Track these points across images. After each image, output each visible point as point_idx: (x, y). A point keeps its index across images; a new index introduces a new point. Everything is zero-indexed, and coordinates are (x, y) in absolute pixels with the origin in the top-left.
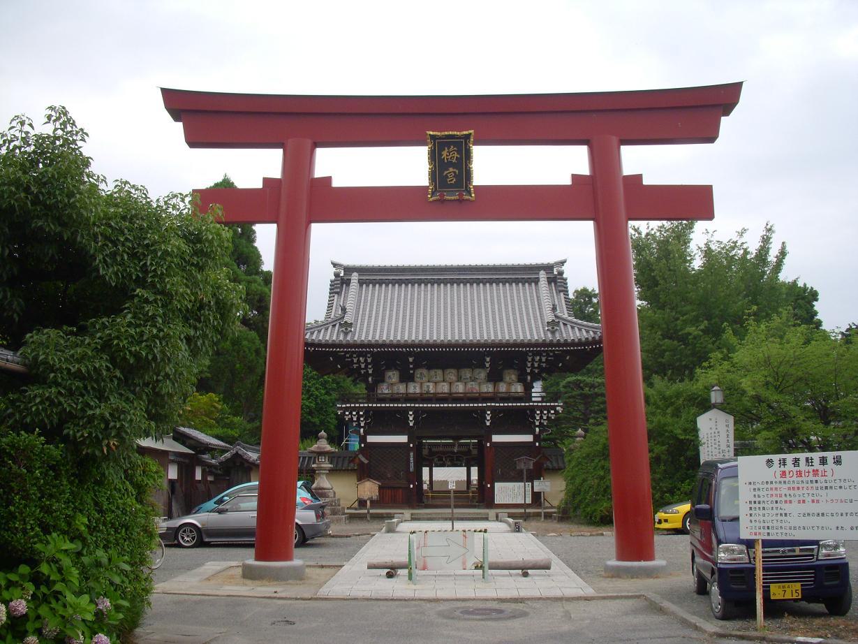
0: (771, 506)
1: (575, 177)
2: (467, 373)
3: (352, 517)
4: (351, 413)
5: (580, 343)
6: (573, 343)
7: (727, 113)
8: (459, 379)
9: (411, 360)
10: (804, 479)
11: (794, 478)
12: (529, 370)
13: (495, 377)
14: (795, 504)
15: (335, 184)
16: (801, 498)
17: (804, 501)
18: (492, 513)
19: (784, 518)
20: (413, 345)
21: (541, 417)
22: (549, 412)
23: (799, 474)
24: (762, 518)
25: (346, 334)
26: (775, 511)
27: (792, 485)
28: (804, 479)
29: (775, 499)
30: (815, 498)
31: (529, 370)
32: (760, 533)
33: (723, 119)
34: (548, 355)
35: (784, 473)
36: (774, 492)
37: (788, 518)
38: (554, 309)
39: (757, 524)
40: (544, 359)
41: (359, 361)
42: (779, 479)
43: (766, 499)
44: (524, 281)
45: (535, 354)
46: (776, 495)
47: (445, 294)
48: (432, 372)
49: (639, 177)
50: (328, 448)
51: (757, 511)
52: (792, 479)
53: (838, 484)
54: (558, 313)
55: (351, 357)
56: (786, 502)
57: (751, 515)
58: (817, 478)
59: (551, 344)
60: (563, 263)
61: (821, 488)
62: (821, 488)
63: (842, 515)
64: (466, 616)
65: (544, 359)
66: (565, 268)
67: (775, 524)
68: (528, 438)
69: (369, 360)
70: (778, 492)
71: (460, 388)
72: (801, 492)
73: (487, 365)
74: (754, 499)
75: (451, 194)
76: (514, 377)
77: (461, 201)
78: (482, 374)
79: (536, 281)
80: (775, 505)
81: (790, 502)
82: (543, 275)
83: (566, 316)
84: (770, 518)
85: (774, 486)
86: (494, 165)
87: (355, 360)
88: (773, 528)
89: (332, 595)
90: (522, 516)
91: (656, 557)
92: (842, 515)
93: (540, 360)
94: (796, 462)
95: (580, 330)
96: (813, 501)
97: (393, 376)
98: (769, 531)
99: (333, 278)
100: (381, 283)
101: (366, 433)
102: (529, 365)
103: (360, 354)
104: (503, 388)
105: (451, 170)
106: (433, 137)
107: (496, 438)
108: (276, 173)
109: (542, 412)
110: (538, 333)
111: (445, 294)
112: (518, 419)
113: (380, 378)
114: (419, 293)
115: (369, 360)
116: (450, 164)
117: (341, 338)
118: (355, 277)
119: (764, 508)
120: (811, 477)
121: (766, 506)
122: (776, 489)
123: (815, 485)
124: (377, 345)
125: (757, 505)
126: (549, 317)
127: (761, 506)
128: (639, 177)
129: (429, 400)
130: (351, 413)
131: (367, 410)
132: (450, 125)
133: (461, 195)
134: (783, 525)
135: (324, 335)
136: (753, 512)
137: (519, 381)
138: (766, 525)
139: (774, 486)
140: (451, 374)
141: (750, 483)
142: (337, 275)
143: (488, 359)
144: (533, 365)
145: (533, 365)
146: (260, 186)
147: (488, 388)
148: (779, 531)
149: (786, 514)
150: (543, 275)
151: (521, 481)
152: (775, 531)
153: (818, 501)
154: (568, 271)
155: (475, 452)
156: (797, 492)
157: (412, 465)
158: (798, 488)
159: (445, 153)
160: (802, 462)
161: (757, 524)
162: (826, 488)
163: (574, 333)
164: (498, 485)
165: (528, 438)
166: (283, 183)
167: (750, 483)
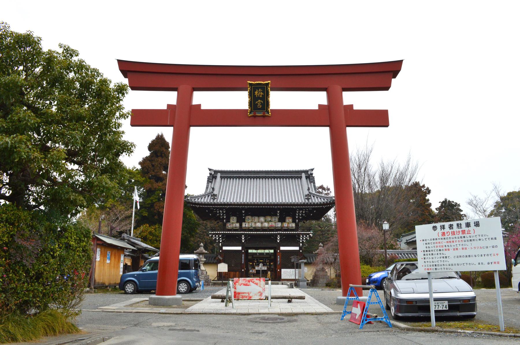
0: (436, 252)
1: (320, 106)
2: (269, 218)
3: (214, 284)
4: (215, 236)
5: (320, 204)
6: (317, 204)
7: (395, 76)
8: (266, 221)
9: (243, 212)
10: (457, 236)
11: (450, 236)
12: (297, 217)
13: (282, 220)
14: (451, 251)
15: (203, 108)
16: (455, 247)
17: (457, 249)
18: (280, 282)
19: (445, 259)
20: (244, 205)
21: (303, 239)
22: (306, 236)
23: (453, 233)
24: (431, 260)
25: (214, 199)
26: (439, 256)
27: (449, 240)
28: (457, 236)
29: (439, 248)
30: (464, 247)
31: (297, 217)
32: (431, 269)
33: (393, 79)
34: (306, 210)
35: (444, 234)
36: (438, 245)
37: (447, 259)
38: (309, 189)
39: (429, 264)
40: (304, 212)
41: (220, 212)
42: (441, 237)
43: (433, 249)
44: (295, 178)
45: (300, 209)
46: (440, 246)
47: (260, 183)
48: (253, 218)
49: (352, 106)
50: (204, 251)
51: (429, 256)
52: (449, 237)
53: (478, 238)
54: (311, 191)
55: (216, 210)
56: (446, 250)
57: (425, 258)
58: (464, 235)
59: (307, 205)
60: (312, 170)
61: (468, 241)
62: (468, 241)
63: (481, 255)
64: (264, 321)
65: (304, 212)
66: (313, 172)
67: (440, 263)
68: (297, 248)
69: (224, 212)
70: (441, 244)
71: (266, 225)
72: (455, 244)
73: (278, 215)
74: (425, 249)
75: (259, 114)
76: (291, 220)
77: (264, 116)
78: (277, 219)
79: (301, 178)
80: (439, 252)
81: (449, 250)
82: (303, 175)
83: (314, 192)
84: (437, 260)
85: (438, 241)
86: (280, 100)
87: (218, 212)
88: (438, 265)
89: (193, 311)
90: (295, 283)
91: (363, 294)
92: (481, 255)
93: (302, 212)
94: (451, 227)
95: (320, 199)
96: (463, 249)
97: (233, 220)
98: (437, 267)
99: (209, 175)
100: (230, 178)
101: (223, 245)
102: (297, 215)
103: (220, 209)
104: (285, 225)
105: (259, 101)
106: (250, 84)
107: (282, 248)
108: (174, 102)
109: (303, 236)
110: (302, 200)
111: (260, 183)
112: (292, 240)
113: (228, 221)
114: (248, 183)
115: (224, 212)
116: (259, 98)
117: (212, 201)
118: (219, 175)
119: (432, 254)
120: (461, 235)
121: (433, 253)
122: (439, 243)
123: (463, 239)
124: (228, 204)
125: (428, 253)
126: (307, 193)
127: (431, 253)
128: (352, 106)
129: (251, 230)
130: (215, 236)
131: (223, 234)
132: (259, 80)
133: (264, 113)
134: (445, 263)
135: (204, 200)
136: (426, 257)
137: (293, 222)
138: (434, 264)
139: (438, 241)
140: (262, 219)
141: (423, 240)
142: (210, 174)
143: (278, 212)
144: (299, 215)
145: (299, 215)
146: (166, 108)
147: (279, 225)
148: (443, 267)
149: (446, 257)
150: (303, 175)
151: (294, 268)
152: (440, 267)
153: (466, 249)
154: (315, 174)
155: (273, 257)
156: (452, 244)
157: (243, 260)
158: (453, 242)
159: (256, 93)
160: (455, 226)
161: (429, 264)
162: (471, 240)
163: (318, 200)
164: (283, 270)
165: (297, 248)
166: (177, 109)
167: (423, 240)
